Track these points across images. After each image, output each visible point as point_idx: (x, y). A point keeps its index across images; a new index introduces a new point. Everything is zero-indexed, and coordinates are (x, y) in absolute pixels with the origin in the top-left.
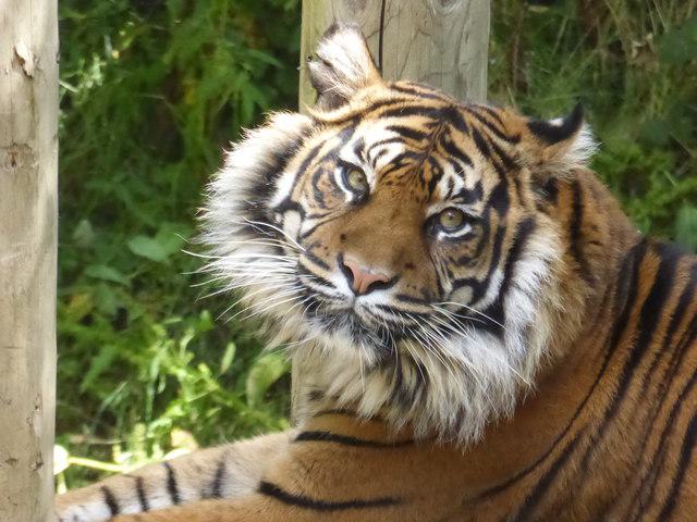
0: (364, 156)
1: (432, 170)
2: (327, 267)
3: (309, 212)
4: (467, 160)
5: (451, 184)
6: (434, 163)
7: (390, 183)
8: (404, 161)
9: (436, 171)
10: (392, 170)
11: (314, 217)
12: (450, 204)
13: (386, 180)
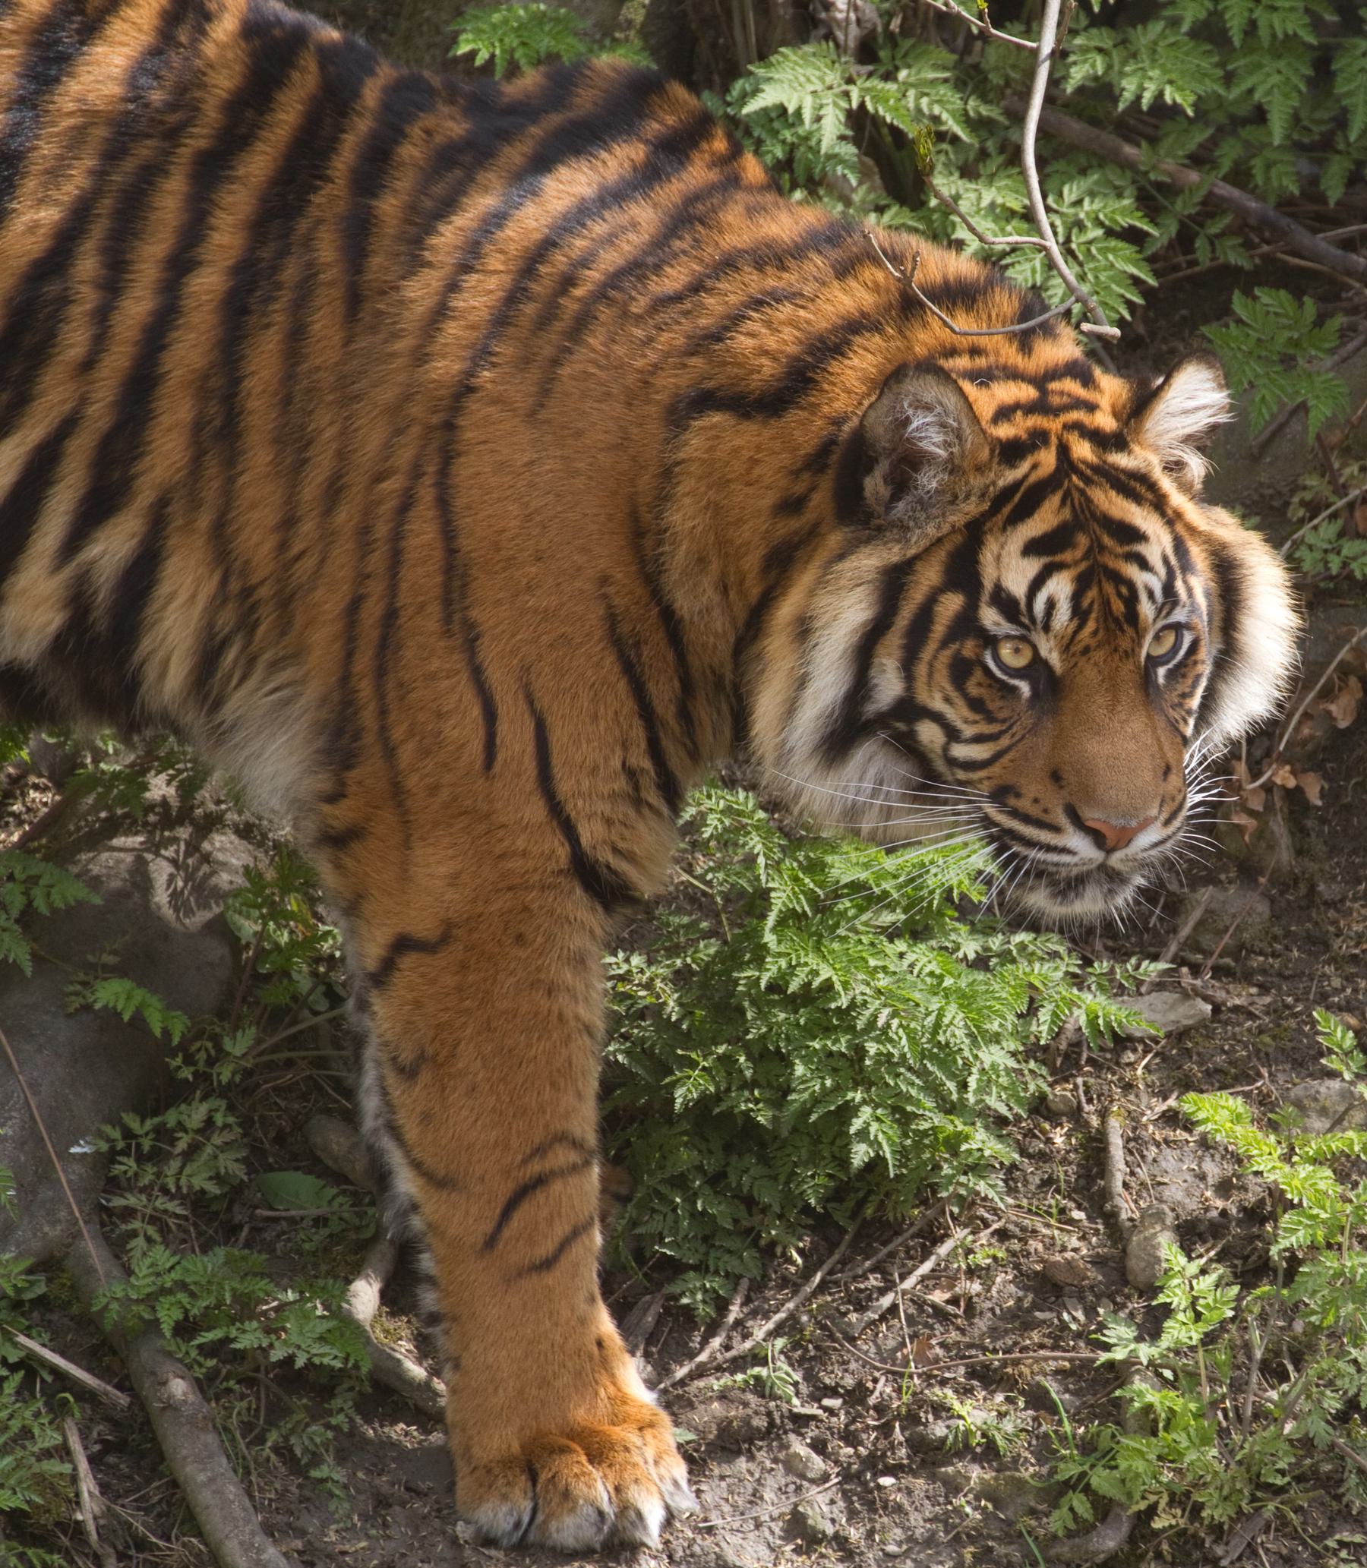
0: (1026, 621)
1: (1119, 595)
2: (1056, 829)
3: (969, 731)
4: (1139, 536)
5: (1151, 595)
6: (1118, 579)
7: (1086, 650)
8: (1086, 603)
9: (1124, 590)
10: (1076, 632)
11: (979, 739)
12: (1160, 624)
13: (1077, 648)
